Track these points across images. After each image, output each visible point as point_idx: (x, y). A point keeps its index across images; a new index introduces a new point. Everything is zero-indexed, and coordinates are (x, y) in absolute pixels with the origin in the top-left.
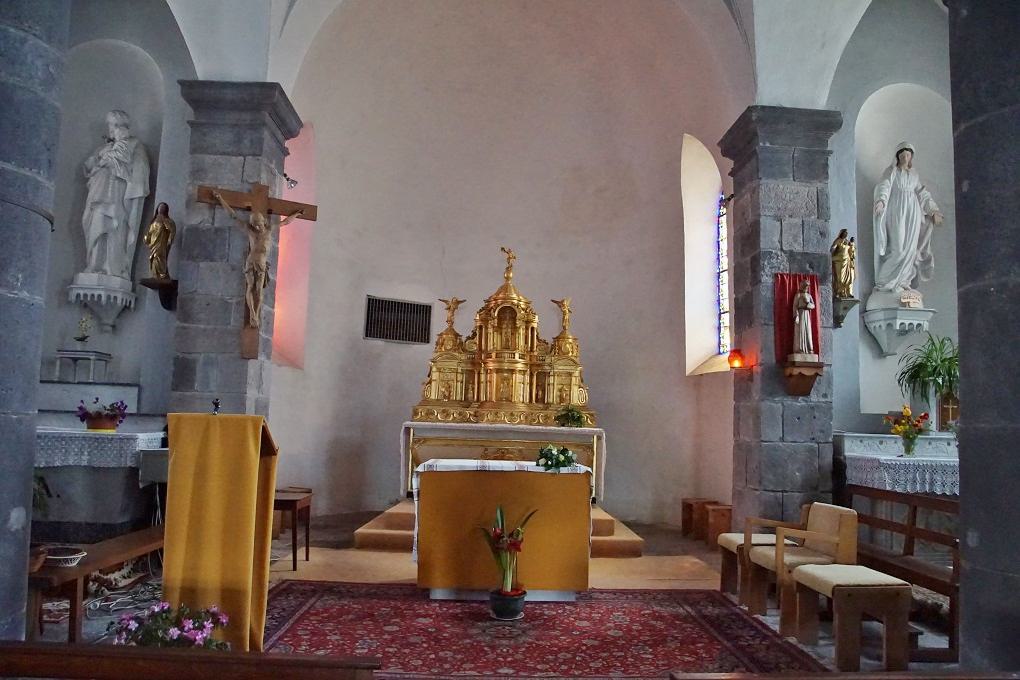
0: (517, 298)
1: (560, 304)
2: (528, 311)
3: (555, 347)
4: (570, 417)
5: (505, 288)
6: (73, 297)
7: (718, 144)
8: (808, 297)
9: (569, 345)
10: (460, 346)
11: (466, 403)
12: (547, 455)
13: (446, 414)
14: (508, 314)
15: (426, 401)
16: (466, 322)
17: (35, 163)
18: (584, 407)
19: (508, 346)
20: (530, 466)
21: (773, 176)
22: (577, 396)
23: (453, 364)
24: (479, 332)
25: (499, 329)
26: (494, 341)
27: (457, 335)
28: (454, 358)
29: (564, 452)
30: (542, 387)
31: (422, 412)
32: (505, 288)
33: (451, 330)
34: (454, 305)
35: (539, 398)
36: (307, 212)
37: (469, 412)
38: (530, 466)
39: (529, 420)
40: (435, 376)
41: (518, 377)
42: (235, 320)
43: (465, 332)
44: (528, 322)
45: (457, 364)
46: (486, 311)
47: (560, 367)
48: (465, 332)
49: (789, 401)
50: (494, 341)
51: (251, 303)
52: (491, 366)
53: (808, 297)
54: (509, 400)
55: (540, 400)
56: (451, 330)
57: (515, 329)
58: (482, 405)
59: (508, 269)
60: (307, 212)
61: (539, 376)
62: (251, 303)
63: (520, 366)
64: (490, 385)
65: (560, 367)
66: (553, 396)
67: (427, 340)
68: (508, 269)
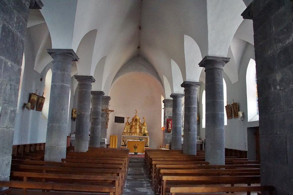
0: (137, 118)
1: (144, 118)
2: (139, 119)
3: (143, 124)
4: (145, 135)
5: (136, 116)
6: (220, 160)
7: (241, 15)
8: (170, 122)
9: (145, 124)
10: (129, 124)
11: (130, 133)
12: (140, 139)
13: (127, 134)
14: (136, 120)
15: (124, 132)
16: (130, 121)
17: (99, 116)
18: (147, 133)
19: (136, 125)
20: (139, 140)
21: (167, 107)
22: (146, 132)
23: (128, 127)
24: (132, 122)
25: (135, 122)
26: (134, 124)
27: (129, 123)
28: (128, 126)
29: (142, 139)
30: (141, 130)
31: (124, 134)
32: (136, 116)
33: (128, 122)
34: (128, 118)
35: (141, 132)
36: (112, 111)
37: (130, 134)
38: (139, 140)
39: (139, 135)
40: (125, 129)
41: (138, 129)
42: (105, 124)
43: (130, 122)
44: (139, 121)
45: (129, 127)
46: (133, 119)
47: (144, 128)
48: (130, 122)
49: (168, 133)
50: (134, 124)
51: (107, 122)
52: (134, 127)
53: (170, 122)
54: (136, 132)
55: (141, 132)
56: (128, 122)
57: (137, 122)
58: (132, 133)
59: (136, 113)
60: (112, 111)
61: (141, 128)
62: (107, 122)
63: (138, 127)
64: (133, 131)
65: (144, 127)
66: (142, 132)
67: (124, 123)
68: (136, 113)
